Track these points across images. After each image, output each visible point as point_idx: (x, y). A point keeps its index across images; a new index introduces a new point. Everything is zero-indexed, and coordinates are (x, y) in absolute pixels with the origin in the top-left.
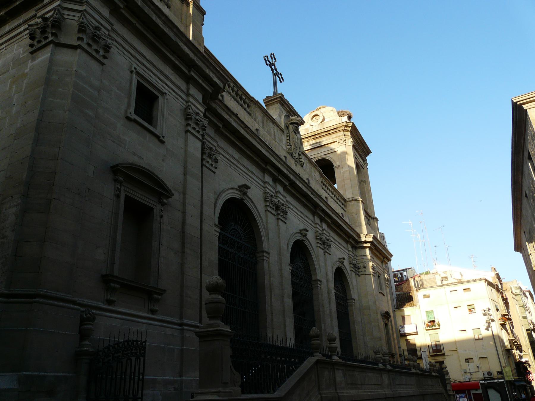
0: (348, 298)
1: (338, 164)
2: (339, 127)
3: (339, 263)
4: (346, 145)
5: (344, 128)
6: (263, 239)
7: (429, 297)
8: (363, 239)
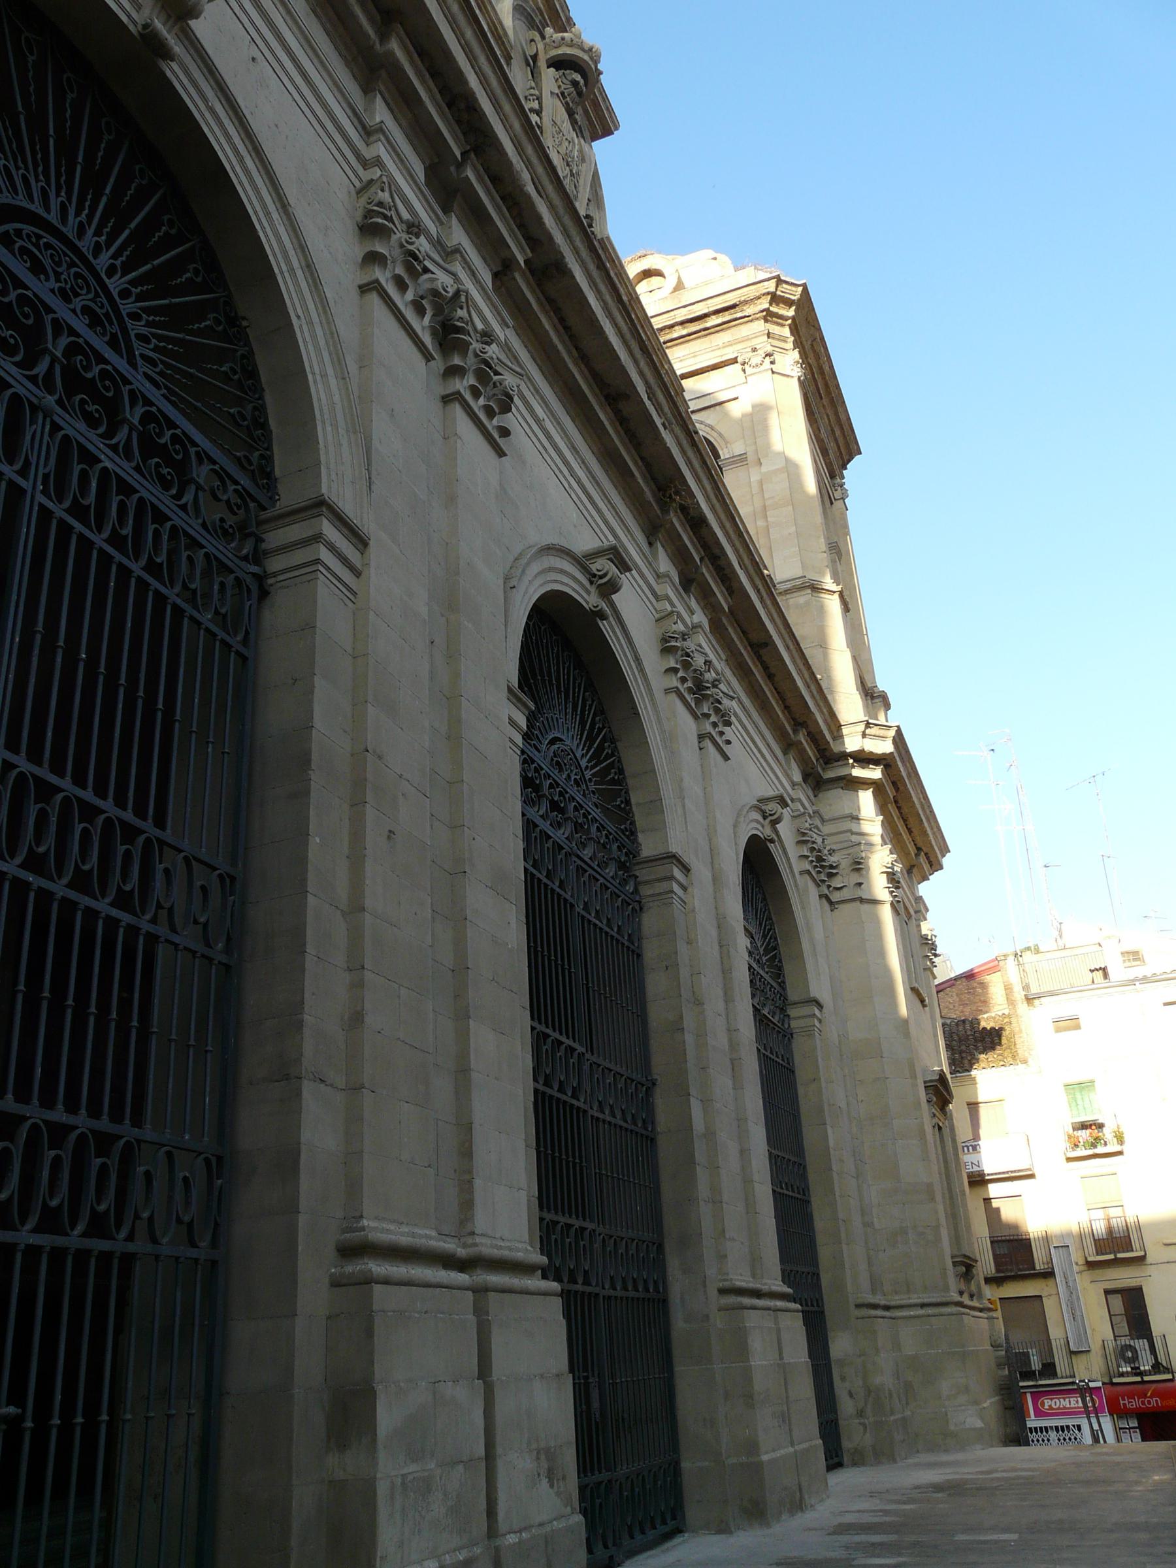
0: (793, 996)
1: (738, 448)
2: (745, 302)
3: (757, 816)
4: (773, 372)
5: (766, 306)
6: (325, 433)
7: (1078, 1027)
8: (852, 742)
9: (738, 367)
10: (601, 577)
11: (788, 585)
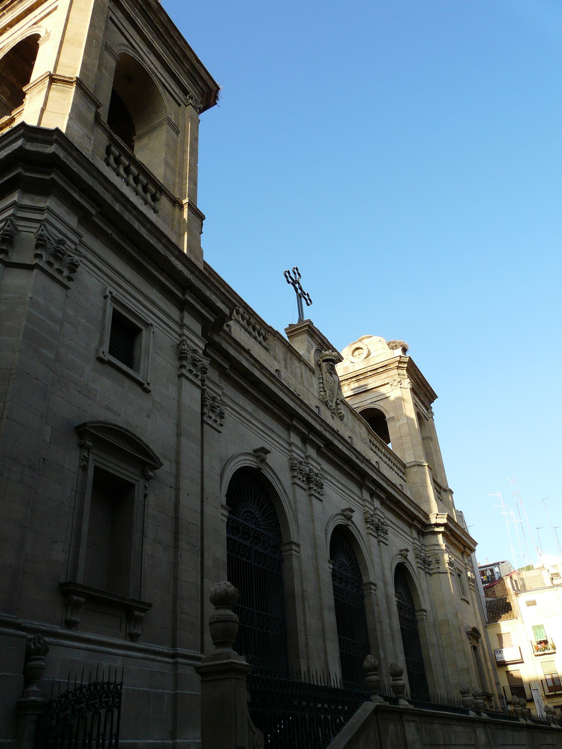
2: (390, 364)
3: (400, 556)
4: (401, 388)
5: (397, 365)
7: (535, 604)
9: (389, 385)
10: (347, 516)
11: (410, 465)
